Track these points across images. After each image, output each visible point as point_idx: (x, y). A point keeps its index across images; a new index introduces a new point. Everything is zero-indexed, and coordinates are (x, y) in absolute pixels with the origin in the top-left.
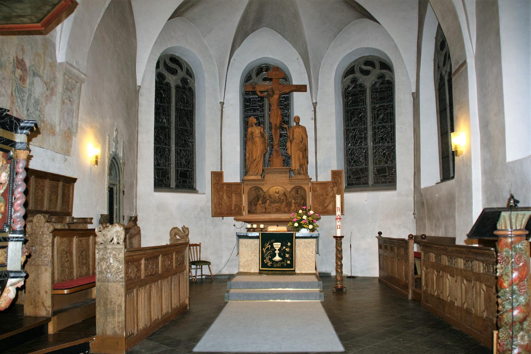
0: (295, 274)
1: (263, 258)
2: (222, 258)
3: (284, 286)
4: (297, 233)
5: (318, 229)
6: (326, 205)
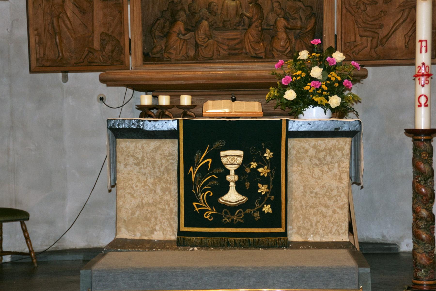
0: (287, 244)
1: (190, 196)
2: (64, 198)
3: (252, 281)
4: (291, 120)
5: (357, 107)
6: (384, 32)
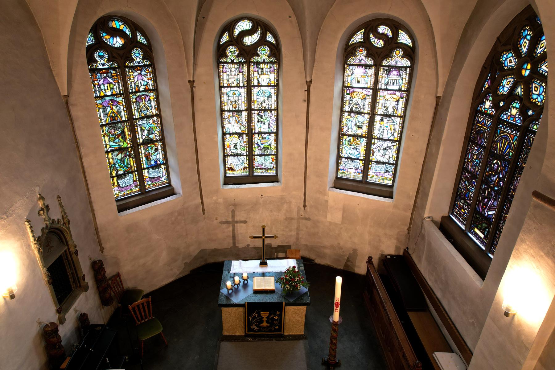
1: (249, 324)
